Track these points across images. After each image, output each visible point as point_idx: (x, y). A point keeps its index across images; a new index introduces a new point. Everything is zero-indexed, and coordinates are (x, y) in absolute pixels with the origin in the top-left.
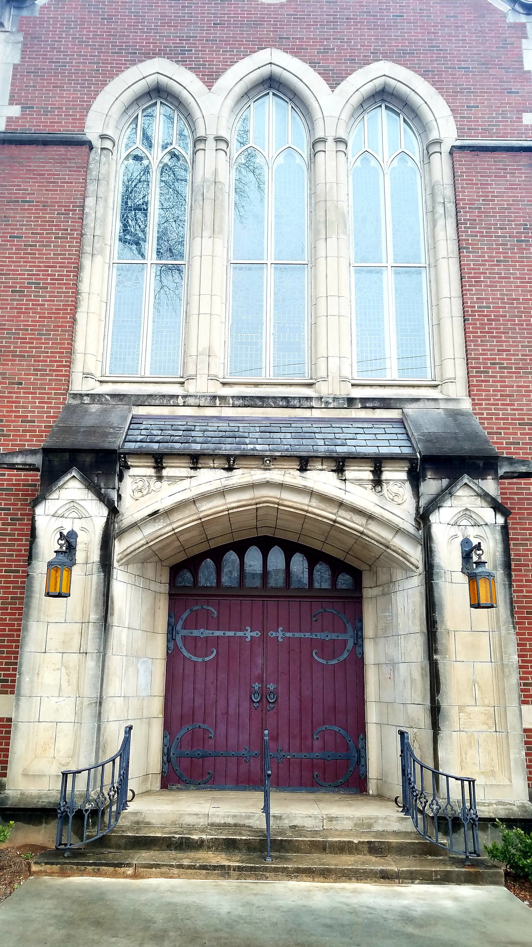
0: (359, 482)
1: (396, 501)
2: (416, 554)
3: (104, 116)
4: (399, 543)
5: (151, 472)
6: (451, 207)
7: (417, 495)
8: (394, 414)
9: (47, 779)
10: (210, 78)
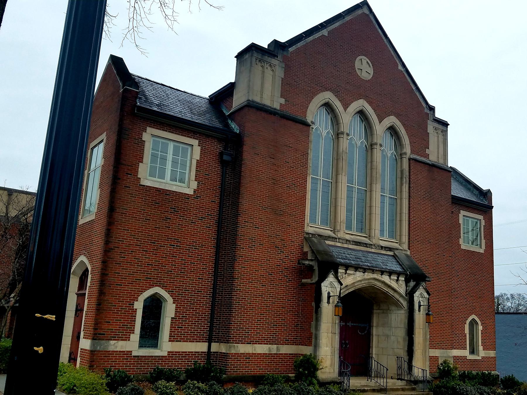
0: (393, 280)
1: (400, 286)
2: (405, 304)
3: (315, 114)
4: (401, 300)
5: (344, 271)
6: (408, 179)
7: (406, 286)
8: (391, 253)
9: (389, 375)
10: (346, 106)
